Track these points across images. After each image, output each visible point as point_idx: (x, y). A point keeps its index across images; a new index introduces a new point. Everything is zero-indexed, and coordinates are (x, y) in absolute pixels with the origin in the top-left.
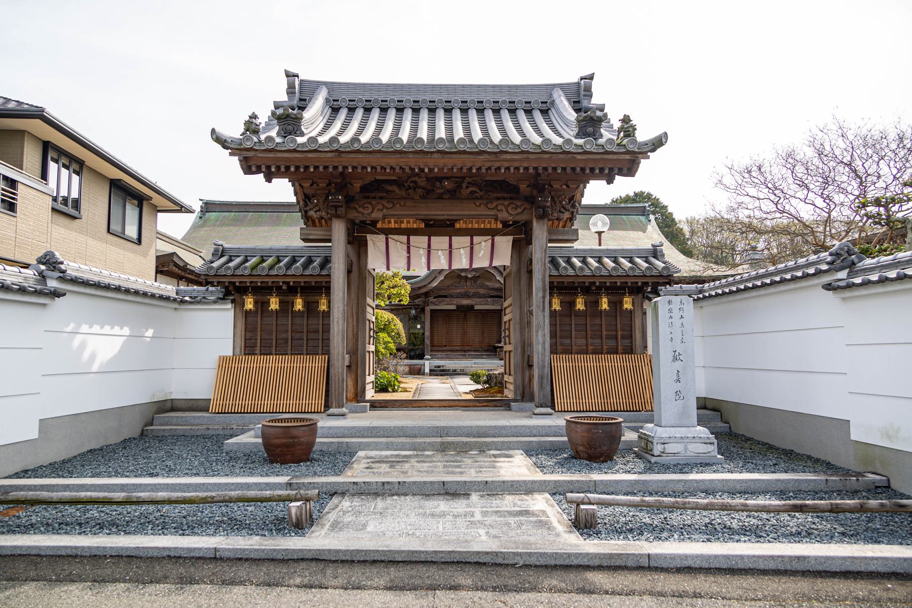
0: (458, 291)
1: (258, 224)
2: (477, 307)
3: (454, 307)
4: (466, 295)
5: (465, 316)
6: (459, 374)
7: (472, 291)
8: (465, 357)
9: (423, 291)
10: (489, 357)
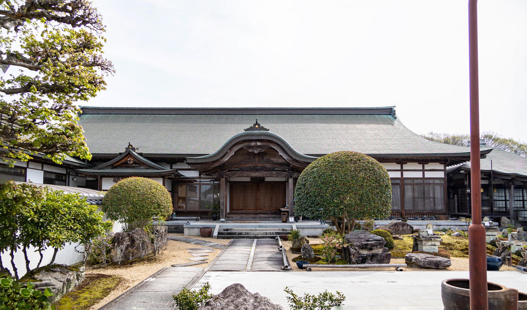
0: (248, 166)
1: (313, 121)
2: (267, 179)
3: (248, 179)
4: (255, 169)
5: (258, 186)
6: (244, 237)
7: (260, 165)
8: (255, 219)
9: (217, 164)
10: (274, 219)
